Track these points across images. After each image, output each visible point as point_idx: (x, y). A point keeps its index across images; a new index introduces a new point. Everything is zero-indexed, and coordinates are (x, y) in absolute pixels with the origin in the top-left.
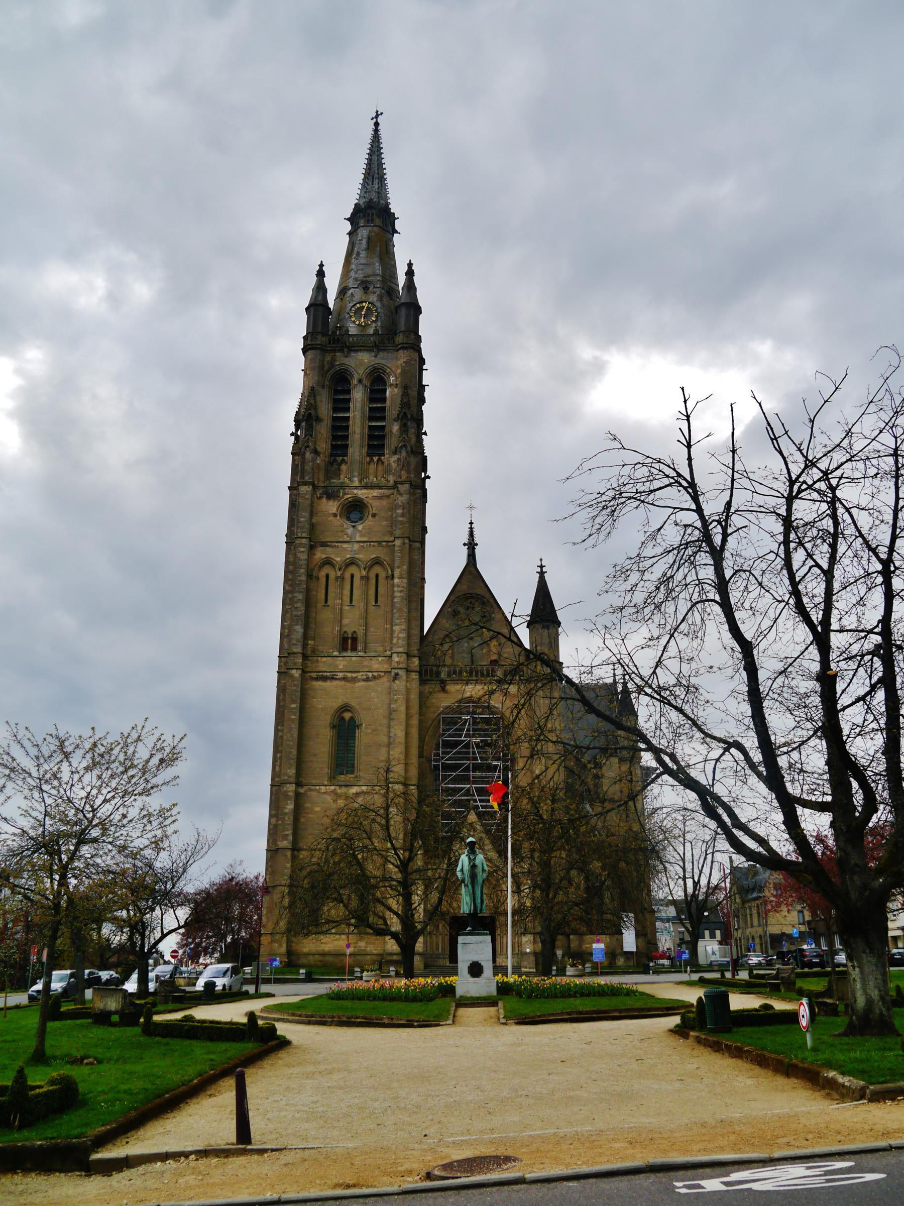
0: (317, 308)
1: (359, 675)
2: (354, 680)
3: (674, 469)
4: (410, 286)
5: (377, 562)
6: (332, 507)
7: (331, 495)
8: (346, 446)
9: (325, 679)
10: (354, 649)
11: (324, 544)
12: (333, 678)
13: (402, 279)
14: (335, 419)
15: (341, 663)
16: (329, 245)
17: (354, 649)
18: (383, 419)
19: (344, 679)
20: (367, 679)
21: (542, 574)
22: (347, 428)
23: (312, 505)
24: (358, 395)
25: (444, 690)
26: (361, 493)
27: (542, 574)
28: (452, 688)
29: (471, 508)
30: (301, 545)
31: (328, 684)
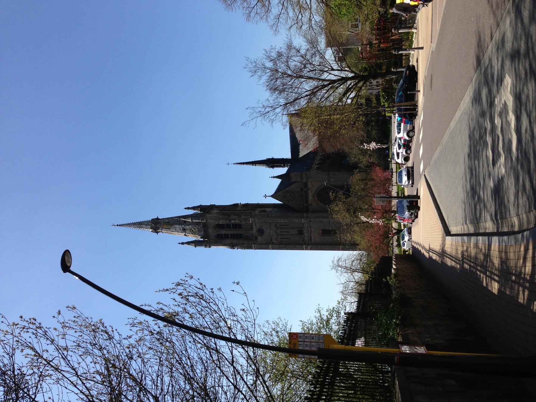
0: (196, 243)
1: (309, 230)
2: (311, 231)
3: (248, 363)
4: (194, 208)
5: (275, 226)
6: (260, 238)
7: (256, 239)
8: (240, 234)
9: (311, 238)
10: (302, 231)
11: (272, 240)
12: (311, 236)
13: (191, 212)
14: (233, 227)
15: (306, 234)
16: (173, 238)
17: (302, 231)
18: (230, 225)
19: (311, 233)
20: (311, 227)
21: (274, 177)
22: (234, 234)
23: (260, 244)
24: (223, 232)
25: (311, 204)
26: (255, 230)
27: (274, 177)
28: (310, 202)
29: (228, 164)
30: (331, 370)
31: (312, 237)
